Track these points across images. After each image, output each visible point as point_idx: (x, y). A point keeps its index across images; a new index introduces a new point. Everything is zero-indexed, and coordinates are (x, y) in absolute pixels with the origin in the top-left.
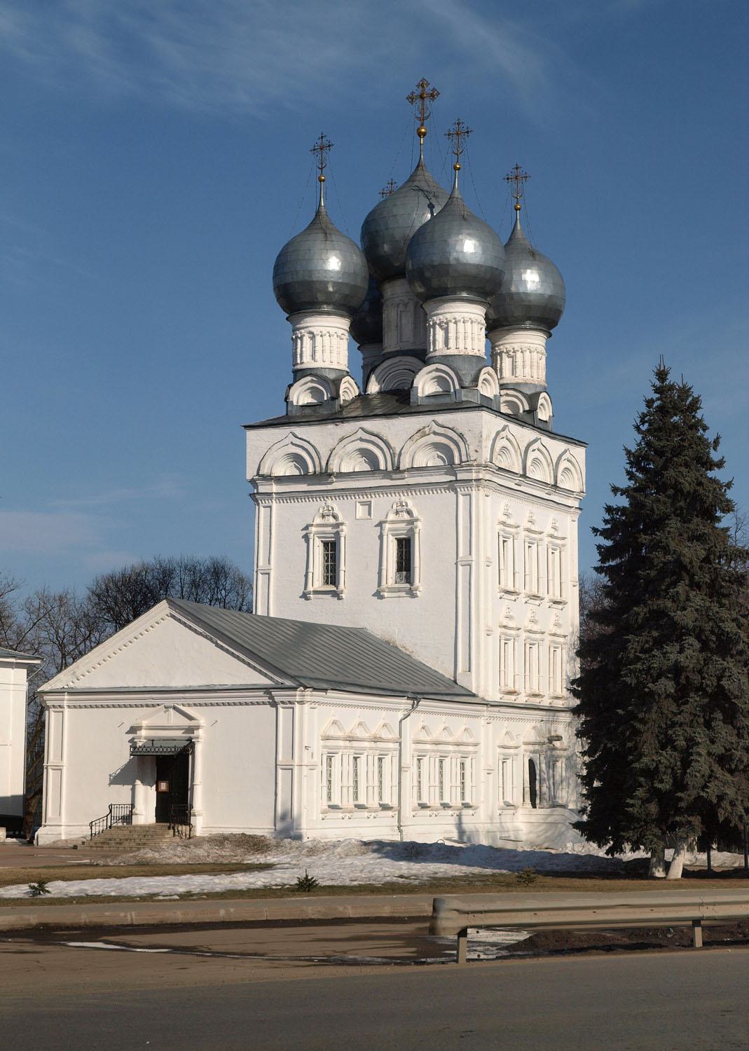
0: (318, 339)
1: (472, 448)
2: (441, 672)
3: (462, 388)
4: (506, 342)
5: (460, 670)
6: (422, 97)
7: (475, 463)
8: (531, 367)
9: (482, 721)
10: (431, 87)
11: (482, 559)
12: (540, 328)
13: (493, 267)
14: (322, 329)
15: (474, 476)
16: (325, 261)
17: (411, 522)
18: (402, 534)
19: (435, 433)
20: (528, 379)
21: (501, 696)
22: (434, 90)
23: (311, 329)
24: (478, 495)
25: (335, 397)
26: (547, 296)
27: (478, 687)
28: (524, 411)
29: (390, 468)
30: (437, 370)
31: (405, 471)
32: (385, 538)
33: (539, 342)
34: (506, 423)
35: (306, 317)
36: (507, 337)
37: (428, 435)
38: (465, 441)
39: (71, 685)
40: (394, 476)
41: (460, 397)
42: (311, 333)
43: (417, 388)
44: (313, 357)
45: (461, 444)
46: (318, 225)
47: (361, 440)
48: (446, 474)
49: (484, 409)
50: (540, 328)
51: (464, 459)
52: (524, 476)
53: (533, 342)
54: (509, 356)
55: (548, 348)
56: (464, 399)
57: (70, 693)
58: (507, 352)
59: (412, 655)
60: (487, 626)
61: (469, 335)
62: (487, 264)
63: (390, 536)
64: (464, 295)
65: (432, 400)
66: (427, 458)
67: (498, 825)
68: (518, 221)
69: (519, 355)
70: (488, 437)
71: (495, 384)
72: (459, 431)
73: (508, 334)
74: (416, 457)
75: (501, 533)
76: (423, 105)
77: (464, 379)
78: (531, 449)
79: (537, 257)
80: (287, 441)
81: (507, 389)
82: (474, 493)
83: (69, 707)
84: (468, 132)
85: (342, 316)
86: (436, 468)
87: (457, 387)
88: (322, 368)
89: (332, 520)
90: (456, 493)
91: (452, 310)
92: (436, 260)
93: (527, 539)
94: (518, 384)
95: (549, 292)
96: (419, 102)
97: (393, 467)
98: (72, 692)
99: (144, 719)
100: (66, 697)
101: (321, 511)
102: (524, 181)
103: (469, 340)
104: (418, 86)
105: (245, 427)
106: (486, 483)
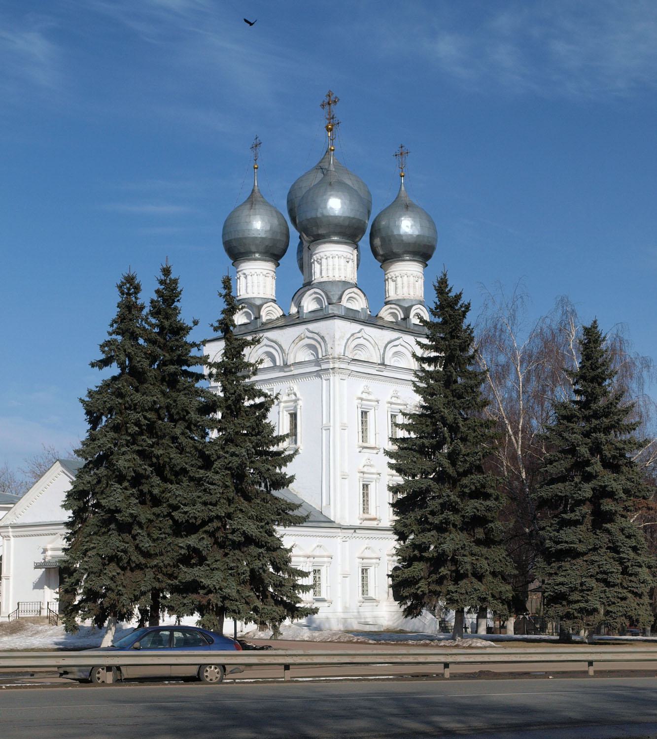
0: (249, 277)
1: (329, 346)
2: (314, 506)
3: (329, 304)
4: (395, 270)
5: (324, 504)
6: (329, 104)
7: (331, 357)
8: (409, 287)
9: (339, 540)
10: (334, 96)
11: (338, 425)
12: (414, 259)
13: (349, 217)
14: (251, 271)
15: (331, 366)
17: (296, 401)
18: (291, 410)
19: (308, 338)
20: (406, 296)
21: (360, 521)
22: (336, 98)
23: (244, 271)
24: (335, 379)
25: (258, 317)
26: (415, 236)
27: (335, 516)
28: (401, 319)
29: (282, 365)
30: (315, 293)
31: (290, 365)
32: (281, 413)
33: (417, 270)
34: (362, 327)
35: (241, 263)
36: (391, 267)
37: (304, 339)
38: (325, 341)
39: (15, 522)
40: (286, 370)
41: (328, 311)
42: (244, 274)
43: (303, 306)
45: (322, 344)
46: (252, 200)
47: (267, 346)
48: (315, 366)
49: (336, 317)
50: (414, 259)
53: (409, 269)
54: (393, 281)
56: (330, 312)
57: (12, 527)
58: (391, 278)
59: (298, 495)
60: (343, 472)
61: (337, 267)
62: (345, 215)
63: (285, 411)
64: (335, 238)
65: (313, 314)
66: (305, 355)
67: (356, 614)
69: (399, 279)
70: (341, 338)
71: (361, 298)
72: (322, 335)
73: (391, 265)
74: (297, 355)
76: (330, 109)
77: (332, 298)
79: (409, 208)
81: (391, 304)
82: (332, 378)
83: (14, 536)
84: (338, 123)
85: (268, 261)
86: (309, 362)
87: (327, 304)
89: (293, 397)
90: (322, 379)
92: (310, 215)
93: (390, 410)
94: (398, 300)
95: (417, 233)
96: (327, 107)
97: (284, 363)
98: (14, 527)
99: (49, 543)
100: (10, 530)
101: (287, 392)
104: (326, 96)
106: (340, 370)
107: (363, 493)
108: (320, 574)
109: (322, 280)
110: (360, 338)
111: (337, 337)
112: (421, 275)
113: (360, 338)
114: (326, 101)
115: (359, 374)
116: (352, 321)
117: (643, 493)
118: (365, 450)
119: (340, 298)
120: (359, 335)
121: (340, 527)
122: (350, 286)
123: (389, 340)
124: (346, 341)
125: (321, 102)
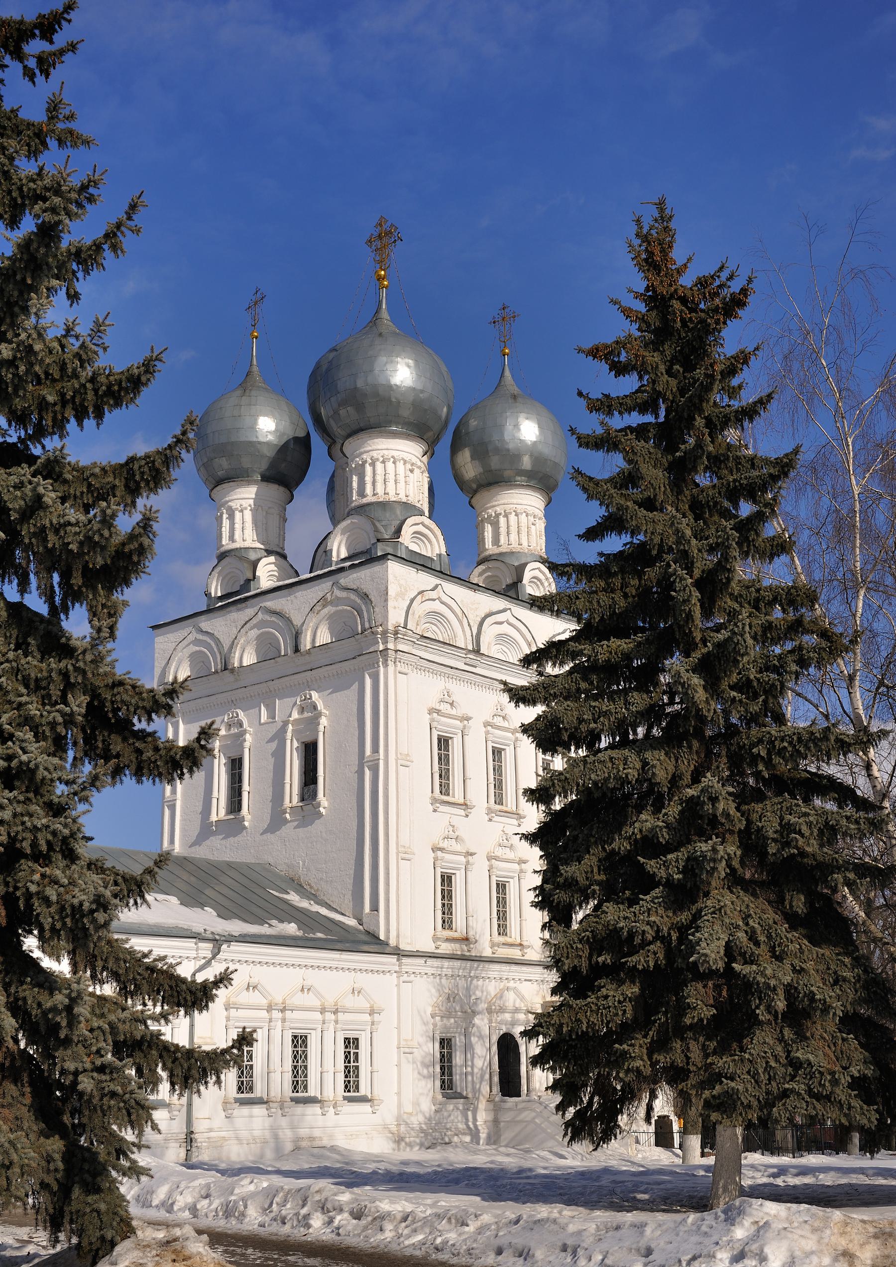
4: (496, 503)
10: (389, 224)
16: (253, 427)
22: (392, 225)
36: (499, 497)
43: (331, 550)
44: (232, 538)
51: (367, 626)
52: (477, 651)
55: (548, 514)
68: (507, 368)
70: (401, 595)
74: (318, 634)
75: (434, 724)
78: (489, 621)
80: (191, 638)
86: (314, 640)
88: (241, 548)
91: (379, 447)
94: (501, 554)
102: (512, 322)
103: (401, 485)
105: (155, 627)
107: (443, 890)
108: (357, 1047)
109: (365, 501)
110: (434, 600)
111: (392, 592)
112: (541, 514)
113: (434, 600)
114: (376, 234)
115: (434, 666)
116: (419, 567)
117: (745, 928)
118: (442, 808)
119: (398, 532)
120: (433, 595)
121: (398, 953)
122: (416, 513)
123: (487, 611)
124: (409, 602)
125: (368, 237)
